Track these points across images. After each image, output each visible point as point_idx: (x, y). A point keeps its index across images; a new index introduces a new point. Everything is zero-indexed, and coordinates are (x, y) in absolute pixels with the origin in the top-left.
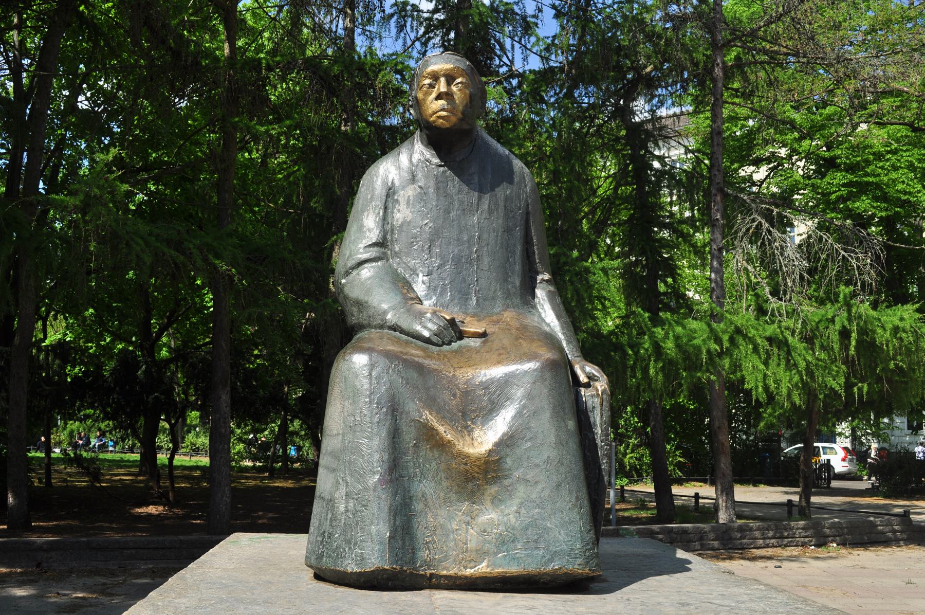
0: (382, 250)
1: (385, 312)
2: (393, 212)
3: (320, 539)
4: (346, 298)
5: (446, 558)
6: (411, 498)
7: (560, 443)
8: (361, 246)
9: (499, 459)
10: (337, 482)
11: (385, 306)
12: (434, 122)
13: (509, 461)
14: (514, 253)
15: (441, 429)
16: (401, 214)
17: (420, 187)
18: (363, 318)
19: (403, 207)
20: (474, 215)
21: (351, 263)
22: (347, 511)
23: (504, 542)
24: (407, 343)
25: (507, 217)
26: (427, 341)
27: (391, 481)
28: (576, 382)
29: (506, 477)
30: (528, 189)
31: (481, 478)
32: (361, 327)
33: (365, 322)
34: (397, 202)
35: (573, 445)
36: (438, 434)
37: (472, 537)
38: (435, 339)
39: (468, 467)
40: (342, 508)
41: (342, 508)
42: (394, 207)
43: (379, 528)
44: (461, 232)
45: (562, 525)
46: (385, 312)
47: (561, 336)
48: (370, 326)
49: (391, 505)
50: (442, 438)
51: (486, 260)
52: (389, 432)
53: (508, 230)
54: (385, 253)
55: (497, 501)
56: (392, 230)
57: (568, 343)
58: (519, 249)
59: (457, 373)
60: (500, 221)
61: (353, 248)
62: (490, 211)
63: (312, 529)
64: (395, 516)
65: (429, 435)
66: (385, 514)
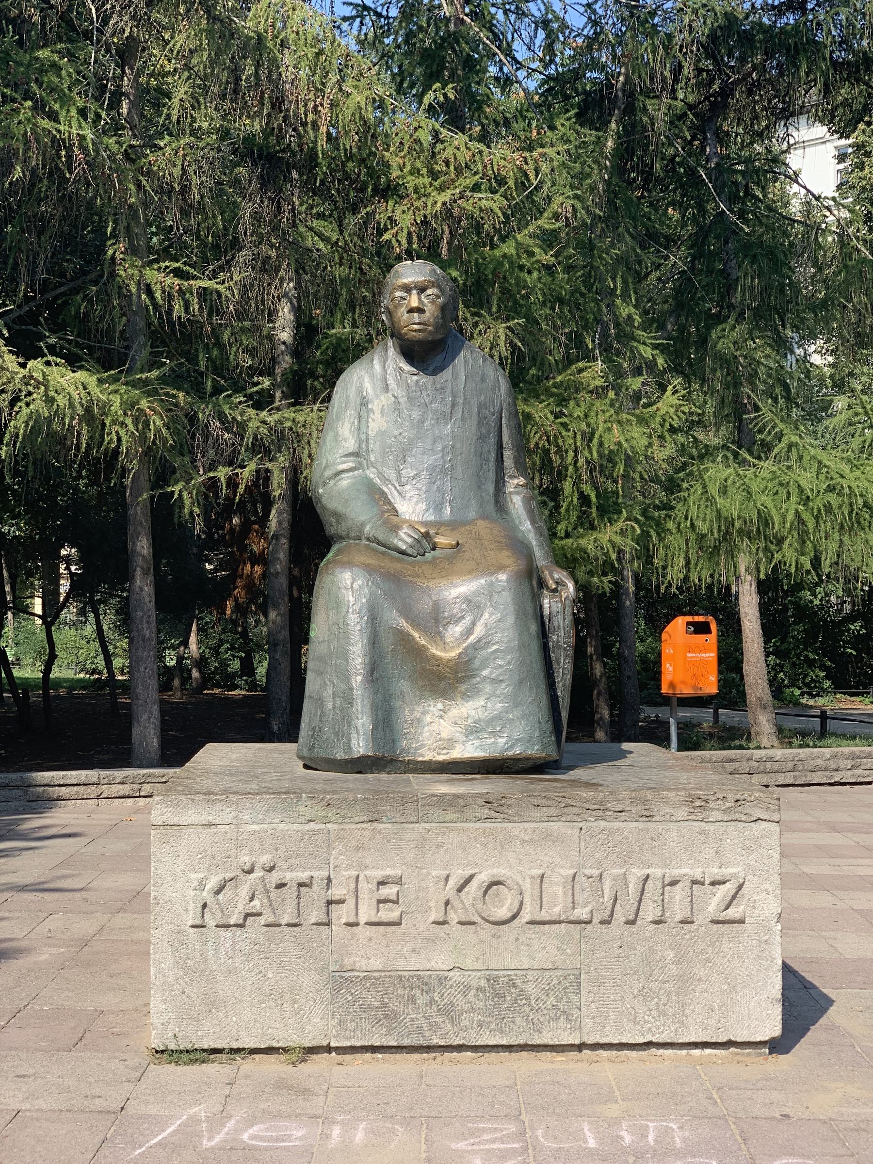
0: (358, 459)
1: (363, 525)
2: (367, 422)
3: (311, 733)
4: (324, 508)
5: (422, 746)
6: (390, 696)
7: (522, 647)
8: (338, 456)
9: (469, 660)
10: (325, 684)
11: (362, 518)
12: (406, 334)
13: (477, 663)
14: (487, 460)
15: (416, 635)
16: (377, 423)
17: (394, 396)
18: (342, 530)
19: (377, 415)
20: (447, 424)
21: (328, 473)
22: (334, 708)
23: (473, 730)
24: (383, 553)
25: (480, 424)
26: (403, 553)
27: (372, 681)
28: (542, 584)
29: (473, 676)
30: (503, 392)
31: (448, 680)
32: (341, 538)
33: (344, 534)
34: (372, 410)
35: (535, 646)
36: (414, 639)
37: (446, 729)
38: (410, 551)
39: (440, 668)
40: (330, 705)
41: (330, 705)
42: (368, 417)
43: (363, 722)
44: (434, 442)
45: (523, 717)
46: (363, 525)
47: (534, 543)
48: (348, 537)
49: (373, 702)
50: (417, 643)
51: (460, 469)
52: (369, 639)
53: (482, 438)
54: (360, 463)
55: (466, 696)
56: (367, 439)
57: (540, 545)
58: (492, 457)
59: (430, 584)
60: (474, 429)
61: (329, 458)
62: (463, 419)
63: (301, 740)
64: (376, 711)
65: (403, 638)
66: (367, 710)
